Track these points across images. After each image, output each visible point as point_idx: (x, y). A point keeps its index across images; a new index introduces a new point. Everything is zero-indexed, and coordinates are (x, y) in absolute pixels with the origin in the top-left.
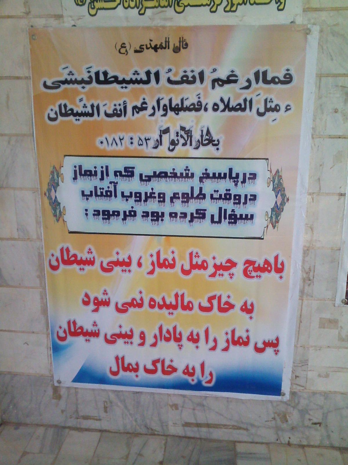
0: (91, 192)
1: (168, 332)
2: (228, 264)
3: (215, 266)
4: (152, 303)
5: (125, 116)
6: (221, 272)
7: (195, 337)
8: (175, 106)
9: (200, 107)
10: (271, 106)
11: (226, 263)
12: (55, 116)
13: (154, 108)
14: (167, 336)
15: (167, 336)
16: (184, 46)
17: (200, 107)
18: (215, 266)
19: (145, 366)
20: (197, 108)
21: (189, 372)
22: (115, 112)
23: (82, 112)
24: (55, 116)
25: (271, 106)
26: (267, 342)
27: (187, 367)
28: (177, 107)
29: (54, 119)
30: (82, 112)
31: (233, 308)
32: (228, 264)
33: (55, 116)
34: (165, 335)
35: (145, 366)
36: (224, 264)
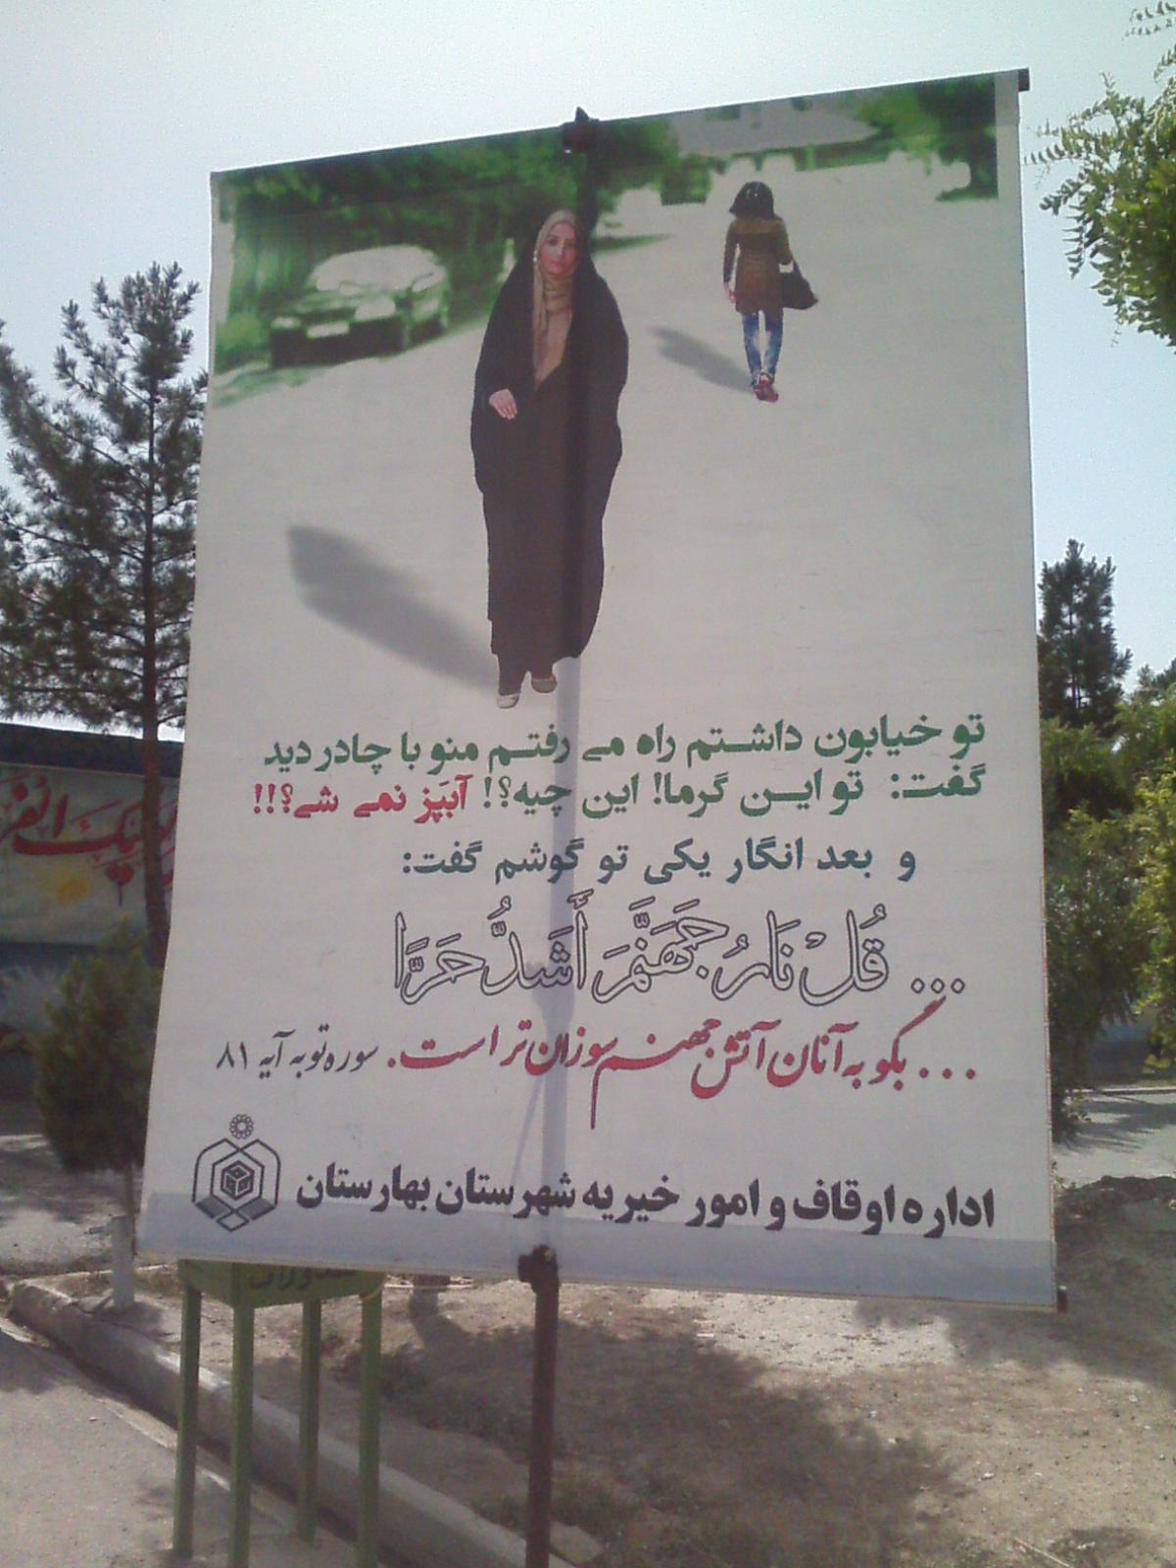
0: (626, 789)
1: (971, 1203)
2: (659, 1198)
3: (630, 1201)
4: (912, 1211)
5: (755, 1213)
6: (644, 1213)
7: (602, 1195)
8: (408, 1186)
9: (853, 1207)
10: (483, 1189)
11: (654, 1195)
12: (316, 1195)
13: (939, 1215)
14: (970, 1212)
15: (970, 1212)
16: (844, 1206)
17: (853, 1207)
18: (630, 1201)
19: (796, 1201)
20: (845, 1210)
21: (530, 1282)
22: (544, 1194)
23: (495, 1190)
24: (316, 1195)
25: (483, 1189)
26: (639, 1197)
27: (594, 1188)
28: (544, 1194)
29: (452, 1210)
30: (495, 1190)
31: (676, 1201)
32: (659, 1198)
33: (454, 1201)
34: (962, 1212)
35: (796, 1201)
36: (649, 1197)
